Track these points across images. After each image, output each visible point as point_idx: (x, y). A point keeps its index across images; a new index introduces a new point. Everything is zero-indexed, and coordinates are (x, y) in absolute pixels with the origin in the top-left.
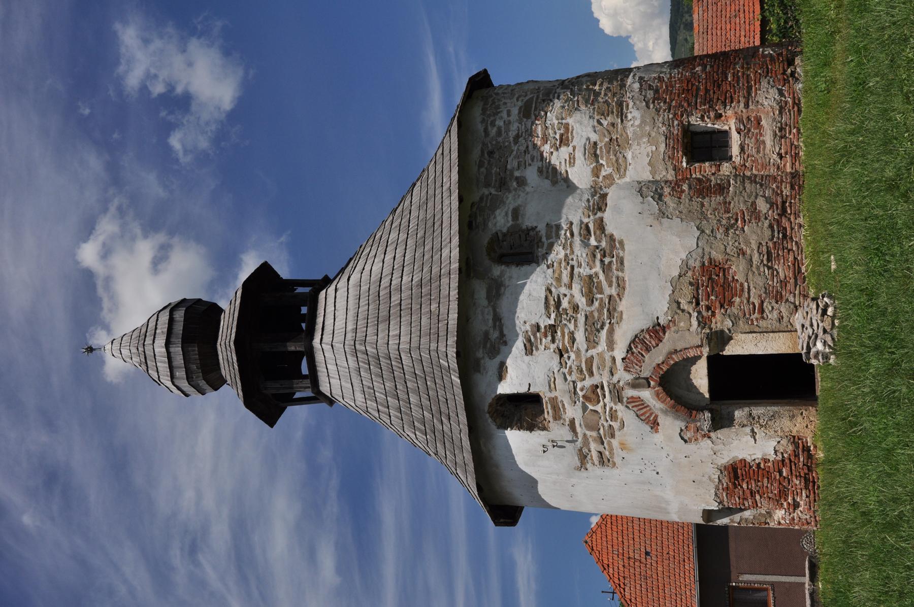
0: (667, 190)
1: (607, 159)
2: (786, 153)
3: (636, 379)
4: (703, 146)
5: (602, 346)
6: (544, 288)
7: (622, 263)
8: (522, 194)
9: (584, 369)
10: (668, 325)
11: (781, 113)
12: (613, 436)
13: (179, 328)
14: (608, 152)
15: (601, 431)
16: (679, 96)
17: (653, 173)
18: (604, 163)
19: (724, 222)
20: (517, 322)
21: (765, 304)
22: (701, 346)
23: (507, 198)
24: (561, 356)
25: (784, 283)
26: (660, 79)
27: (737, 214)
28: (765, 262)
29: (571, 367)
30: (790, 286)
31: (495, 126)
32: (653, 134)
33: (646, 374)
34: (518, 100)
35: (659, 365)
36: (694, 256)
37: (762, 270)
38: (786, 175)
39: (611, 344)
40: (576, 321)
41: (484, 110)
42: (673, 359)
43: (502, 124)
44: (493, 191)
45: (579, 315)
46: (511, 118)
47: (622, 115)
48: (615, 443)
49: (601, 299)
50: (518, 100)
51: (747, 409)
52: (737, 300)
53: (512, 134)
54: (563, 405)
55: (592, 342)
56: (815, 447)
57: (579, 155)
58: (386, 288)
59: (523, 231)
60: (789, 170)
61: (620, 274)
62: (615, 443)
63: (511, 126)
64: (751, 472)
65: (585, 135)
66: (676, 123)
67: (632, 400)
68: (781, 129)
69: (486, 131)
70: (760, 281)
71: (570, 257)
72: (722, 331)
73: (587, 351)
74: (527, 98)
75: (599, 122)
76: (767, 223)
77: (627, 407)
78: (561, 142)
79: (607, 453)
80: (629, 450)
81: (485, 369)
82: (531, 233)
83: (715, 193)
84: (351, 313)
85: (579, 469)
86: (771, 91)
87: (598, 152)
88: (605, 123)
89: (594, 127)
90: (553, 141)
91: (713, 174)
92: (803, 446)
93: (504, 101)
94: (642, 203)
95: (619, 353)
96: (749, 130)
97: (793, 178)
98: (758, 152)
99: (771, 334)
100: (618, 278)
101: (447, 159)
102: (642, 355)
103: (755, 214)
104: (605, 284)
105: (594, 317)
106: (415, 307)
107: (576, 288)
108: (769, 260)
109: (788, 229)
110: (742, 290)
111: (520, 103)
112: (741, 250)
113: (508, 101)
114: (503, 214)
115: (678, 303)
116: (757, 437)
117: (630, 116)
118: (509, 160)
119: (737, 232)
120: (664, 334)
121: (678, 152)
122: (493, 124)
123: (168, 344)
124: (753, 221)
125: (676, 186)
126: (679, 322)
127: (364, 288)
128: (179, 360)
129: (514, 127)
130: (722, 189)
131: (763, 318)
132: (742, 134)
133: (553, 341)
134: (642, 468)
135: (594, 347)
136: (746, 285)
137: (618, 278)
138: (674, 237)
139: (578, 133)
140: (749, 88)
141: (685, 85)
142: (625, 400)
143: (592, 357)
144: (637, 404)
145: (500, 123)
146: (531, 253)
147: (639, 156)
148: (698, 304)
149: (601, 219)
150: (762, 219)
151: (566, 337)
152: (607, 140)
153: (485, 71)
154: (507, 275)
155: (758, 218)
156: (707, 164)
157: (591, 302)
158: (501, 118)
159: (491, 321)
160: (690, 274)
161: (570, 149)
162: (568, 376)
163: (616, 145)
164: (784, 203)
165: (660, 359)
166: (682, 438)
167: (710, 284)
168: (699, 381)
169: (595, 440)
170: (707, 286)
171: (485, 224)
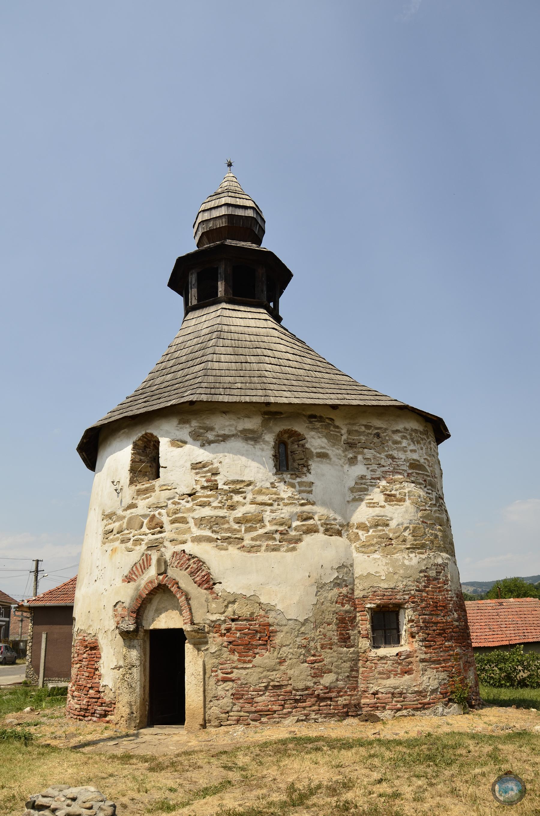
0: (344, 590)
1: (373, 536)
2: (378, 699)
3: (166, 562)
4: (385, 622)
5: (196, 532)
6: (252, 479)
7: (274, 550)
8: (341, 462)
9: (177, 516)
10: (214, 593)
11: (416, 692)
12: (122, 542)
13: (240, 212)
14: (380, 537)
15: (126, 532)
16: (431, 598)
17: (361, 577)
18: (370, 533)
19: (312, 644)
20: (221, 455)
21: (231, 683)
22: (192, 623)
23: (338, 449)
24: (190, 495)
25: (251, 701)
26: (445, 583)
27: (320, 656)
28: (272, 684)
29: (179, 503)
30: (248, 707)
31: (402, 439)
32: (396, 577)
33: (171, 572)
34: (425, 459)
35: (177, 583)
36: (279, 617)
37: (264, 680)
38: (357, 699)
39: (198, 540)
40: (220, 507)
41: (416, 431)
42: (181, 597)
43: (404, 444)
44: (344, 437)
45: (225, 510)
46: (409, 452)
47: (413, 548)
48: (117, 544)
49: (240, 531)
50: (425, 459)
51: (138, 663)
52: (236, 657)
53: (395, 453)
54: (148, 498)
55: (200, 522)
56: (108, 722)
57: (377, 511)
58: (263, 353)
59: (306, 461)
60: (363, 701)
61: (263, 548)
62: (117, 544)
63: (402, 452)
64: (92, 663)
65: (396, 515)
66: (407, 597)
67: (148, 559)
68: (401, 694)
69: (397, 431)
70: (253, 679)
72: (206, 643)
73: (193, 518)
74: (427, 467)
75: (406, 529)
77: (143, 554)
78: (389, 495)
79: (111, 537)
80: (111, 556)
81: (181, 428)
82: (305, 469)
83: (341, 634)
84: (246, 330)
85: (103, 512)
86: (436, 682)
87: (380, 528)
88: (406, 534)
89: (402, 524)
90: (390, 488)
91: (359, 632)
92: (108, 711)
93: (424, 448)
94: (332, 568)
95: (190, 548)
96: (399, 664)
97: (355, 706)
98: (380, 673)
99: (202, 689)
100: (260, 546)
101: (372, 398)
102: (187, 568)
103: (318, 674)
104: (254, 534)
105: (223, 524)
106: (242, 373)
107: (252, 508)
108: (274, 687)
109: (304, 704)
110: (245, 662)
111: (422, 461)
113: (424, 451)
114: (323, 445)
115: (234, 602)
116: (116, 671)
118: (372, 451)
119: (302, 657)
120: (206, 589)
121: (380, 599)
122: (404, 437)
123: (227, 205)
124: (313, 671)
125: (349, 598)
126: (216, 603)
127: (266, 339)
128: (216, 213)
129: (401, 455)
130: (345, 640)
131: (218, 681)
132: (396, 658)
133: (203, 488)
134: (100, 568)
135: (196, 525)
136: (250, 665)
137: (260, 546)
138: (298, 598)
139: (396, 509)
140: (438, 662)
141: (441, 603)
142: (149, 552)
143: (188, 523)
144: (144, 564)
145: (405, 443)
146: (288, 469)
147: (376, 564)
148: (233, 620)
149: (317, 531)
150: (314, 680)
151: (205, 499)
152: (391, 536)
153: (449, 436)
154: (265, 447)
155: (315, 676)
156: (369, 626)
157: (238, 521)
158: (409, 445)
159: (223, 432)
160: (262, 613)
161: (382, 503)
162: (171, 501)
163: (387, 543)
164: (331, 699)
165: (182, 585)
166: (117, 603)
167: (252, 634)
168: (164, 621)
169: (121, 526)
170: (249, 629)
171: (313, 429)
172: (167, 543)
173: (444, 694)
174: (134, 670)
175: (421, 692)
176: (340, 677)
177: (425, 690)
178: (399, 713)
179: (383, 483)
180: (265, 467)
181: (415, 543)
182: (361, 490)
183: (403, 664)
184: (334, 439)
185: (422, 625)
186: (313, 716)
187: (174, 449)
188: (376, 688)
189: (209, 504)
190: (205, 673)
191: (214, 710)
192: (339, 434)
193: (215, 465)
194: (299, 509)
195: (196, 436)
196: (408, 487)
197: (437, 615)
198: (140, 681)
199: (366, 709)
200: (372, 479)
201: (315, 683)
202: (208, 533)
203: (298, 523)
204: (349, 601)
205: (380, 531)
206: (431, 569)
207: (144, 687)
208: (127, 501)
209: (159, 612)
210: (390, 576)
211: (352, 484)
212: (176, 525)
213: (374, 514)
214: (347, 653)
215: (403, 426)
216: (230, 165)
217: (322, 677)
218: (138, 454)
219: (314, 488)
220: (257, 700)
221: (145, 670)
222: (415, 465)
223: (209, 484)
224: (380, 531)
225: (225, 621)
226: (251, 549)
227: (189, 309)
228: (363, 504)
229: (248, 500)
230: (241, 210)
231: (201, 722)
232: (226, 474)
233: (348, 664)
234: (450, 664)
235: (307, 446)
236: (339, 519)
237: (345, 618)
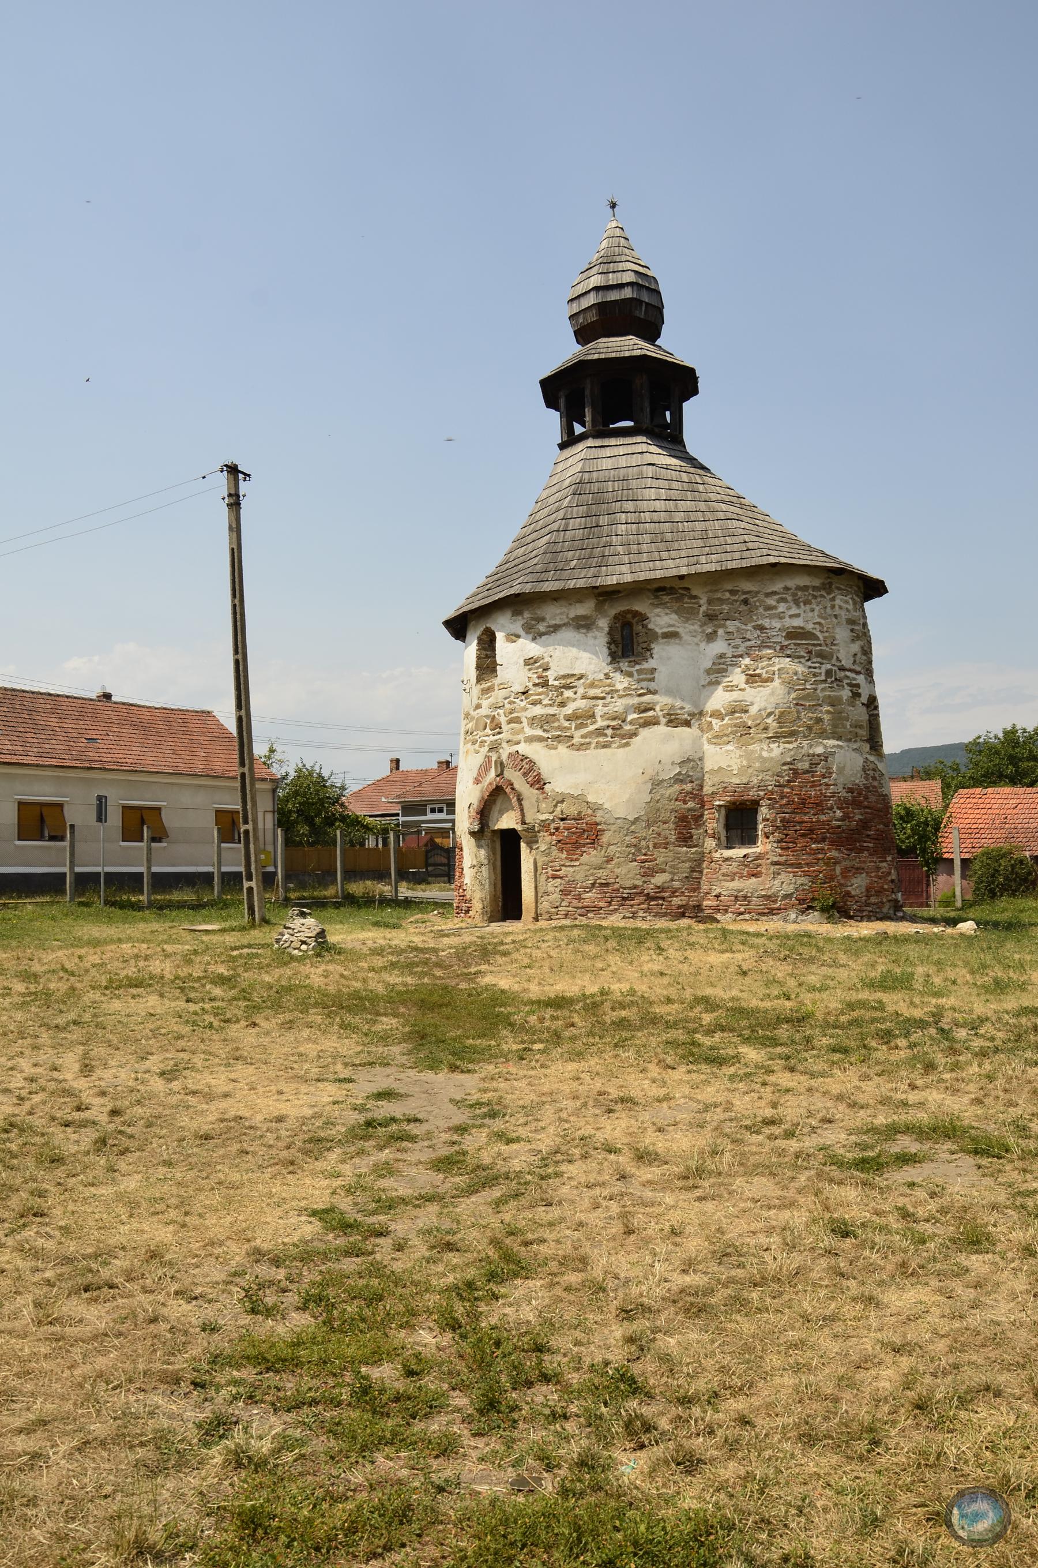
0: (688, 787)
5: (529, 732)
6: (583, 672)
7: (604, 747)
8: (696, 640)
11: (763, 896)
13: (614, 296)
14: (735, 726)
19: (643, 843)
20: (551, 648)
22: (523, 823)
25: (578, 897)
29: (514, 703)
30: (575, 902)
32: (750, 771)
36: (607, 816)
38: (698, 901)
39: (530, 740)
41: (805, 588)
44: (703, 609)
46: (787, 618)
47: (777, 737)
49: (570, 728)
51: (486, 862)
53: (766, 623)
55: (532, 721)
57: (736, 695)
60: (705, 903)
61: (593, 745)
66: (762, 793)
68: (745, 897)
69: (774, 593)
70: (580, 877)
71: (615, 695)
75: (769, 715)
76: (639, 883)
78: (751, 675)
86: (791, 887)
87: (737, 715)
88: (769, 721)
89: (765, 709)
94: (673, 763)
95: (523, 748)
98: (724, 875)
100: (590, 743)
104: (584, 731)
108: (601, 884)
109: (632, 902)
112: (612, 859)
115: (562, 802)
117: (773, 746)
122: (783, 600)
123: (597, 289)
124: (642, 870)
125: (697, 795)
129: (777, 624)
130: (685, 839)
131: (548, 878)
133: (535, 685)
139: (759, 692)
140: (799, 866)
145: (782, 607)
148: (562, 819)
149: (657, 723)
150: (643, 879)
151: (537, 697)
152: (750, 724)
155: (645, 875)
157: (568, 719)
158: (789, 608)
159: (554, 622)
160: (590, 812)
161: (743, 686)
164: (663, 899)
165: (516, 786)
167: (581, 832)
171: (657, 606)
172: (504, 745)
173: (801, 901)
174: (483, 868)
175: (770, 896)
176: (676, 878)
177: (775, 895)
178: (742, 917)
179: (747, 661)
180: (598, 657)
181: (780, 730)
182: (719, 671)
183: (752, 868)
184: (687, 614)
185: (778, 824)
186: (641, 914)
187: (509, 644)
188: (718, 891)
189: (540, 702)
190: (536, 870)
191: (545, 905)
192: (696, 606)
193: (546, 660)
194: (636, 700)
195: (528, 628)
196: (779, 663)
197: (806, 814)
198: (489, 878)
199: (707, 912)
200: (735, 657)
201: (645, 882)
202: (539, 732)
203: (636, 716)
204: (694, 798)
205: (737, 718)
206: (800, 760)
207: (495, 884)
208: (475, 701)
209: (501, 813)
210: (742, 770)
211: (708, 664)
212: (512, 725)
213: (731, 699)
214: (687, 853)
215: (782, 586)
216: (613, 206)
217: (653, 876)
218: (484, 649)
219: (656, 675)
220: (583, 896)
221: (494, 868)
222: (795, 634)
223: (540, 680)
224: (737, 718)
225: (553, 821)
226: (581, 747)
227: (569, 441)
228: (720, 687)
229: (579, 695)
230: (615, 291)
231: (533, 915)
232: (557, 669)
233: (687, 865)
234: (816, 868)
235: (650, 626)
236: (688, 707)
237: (687, 817)
